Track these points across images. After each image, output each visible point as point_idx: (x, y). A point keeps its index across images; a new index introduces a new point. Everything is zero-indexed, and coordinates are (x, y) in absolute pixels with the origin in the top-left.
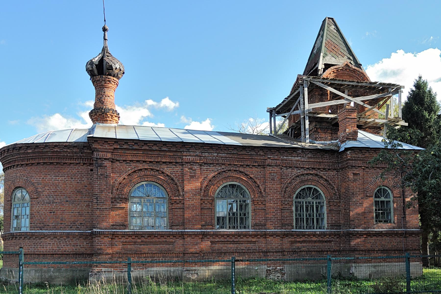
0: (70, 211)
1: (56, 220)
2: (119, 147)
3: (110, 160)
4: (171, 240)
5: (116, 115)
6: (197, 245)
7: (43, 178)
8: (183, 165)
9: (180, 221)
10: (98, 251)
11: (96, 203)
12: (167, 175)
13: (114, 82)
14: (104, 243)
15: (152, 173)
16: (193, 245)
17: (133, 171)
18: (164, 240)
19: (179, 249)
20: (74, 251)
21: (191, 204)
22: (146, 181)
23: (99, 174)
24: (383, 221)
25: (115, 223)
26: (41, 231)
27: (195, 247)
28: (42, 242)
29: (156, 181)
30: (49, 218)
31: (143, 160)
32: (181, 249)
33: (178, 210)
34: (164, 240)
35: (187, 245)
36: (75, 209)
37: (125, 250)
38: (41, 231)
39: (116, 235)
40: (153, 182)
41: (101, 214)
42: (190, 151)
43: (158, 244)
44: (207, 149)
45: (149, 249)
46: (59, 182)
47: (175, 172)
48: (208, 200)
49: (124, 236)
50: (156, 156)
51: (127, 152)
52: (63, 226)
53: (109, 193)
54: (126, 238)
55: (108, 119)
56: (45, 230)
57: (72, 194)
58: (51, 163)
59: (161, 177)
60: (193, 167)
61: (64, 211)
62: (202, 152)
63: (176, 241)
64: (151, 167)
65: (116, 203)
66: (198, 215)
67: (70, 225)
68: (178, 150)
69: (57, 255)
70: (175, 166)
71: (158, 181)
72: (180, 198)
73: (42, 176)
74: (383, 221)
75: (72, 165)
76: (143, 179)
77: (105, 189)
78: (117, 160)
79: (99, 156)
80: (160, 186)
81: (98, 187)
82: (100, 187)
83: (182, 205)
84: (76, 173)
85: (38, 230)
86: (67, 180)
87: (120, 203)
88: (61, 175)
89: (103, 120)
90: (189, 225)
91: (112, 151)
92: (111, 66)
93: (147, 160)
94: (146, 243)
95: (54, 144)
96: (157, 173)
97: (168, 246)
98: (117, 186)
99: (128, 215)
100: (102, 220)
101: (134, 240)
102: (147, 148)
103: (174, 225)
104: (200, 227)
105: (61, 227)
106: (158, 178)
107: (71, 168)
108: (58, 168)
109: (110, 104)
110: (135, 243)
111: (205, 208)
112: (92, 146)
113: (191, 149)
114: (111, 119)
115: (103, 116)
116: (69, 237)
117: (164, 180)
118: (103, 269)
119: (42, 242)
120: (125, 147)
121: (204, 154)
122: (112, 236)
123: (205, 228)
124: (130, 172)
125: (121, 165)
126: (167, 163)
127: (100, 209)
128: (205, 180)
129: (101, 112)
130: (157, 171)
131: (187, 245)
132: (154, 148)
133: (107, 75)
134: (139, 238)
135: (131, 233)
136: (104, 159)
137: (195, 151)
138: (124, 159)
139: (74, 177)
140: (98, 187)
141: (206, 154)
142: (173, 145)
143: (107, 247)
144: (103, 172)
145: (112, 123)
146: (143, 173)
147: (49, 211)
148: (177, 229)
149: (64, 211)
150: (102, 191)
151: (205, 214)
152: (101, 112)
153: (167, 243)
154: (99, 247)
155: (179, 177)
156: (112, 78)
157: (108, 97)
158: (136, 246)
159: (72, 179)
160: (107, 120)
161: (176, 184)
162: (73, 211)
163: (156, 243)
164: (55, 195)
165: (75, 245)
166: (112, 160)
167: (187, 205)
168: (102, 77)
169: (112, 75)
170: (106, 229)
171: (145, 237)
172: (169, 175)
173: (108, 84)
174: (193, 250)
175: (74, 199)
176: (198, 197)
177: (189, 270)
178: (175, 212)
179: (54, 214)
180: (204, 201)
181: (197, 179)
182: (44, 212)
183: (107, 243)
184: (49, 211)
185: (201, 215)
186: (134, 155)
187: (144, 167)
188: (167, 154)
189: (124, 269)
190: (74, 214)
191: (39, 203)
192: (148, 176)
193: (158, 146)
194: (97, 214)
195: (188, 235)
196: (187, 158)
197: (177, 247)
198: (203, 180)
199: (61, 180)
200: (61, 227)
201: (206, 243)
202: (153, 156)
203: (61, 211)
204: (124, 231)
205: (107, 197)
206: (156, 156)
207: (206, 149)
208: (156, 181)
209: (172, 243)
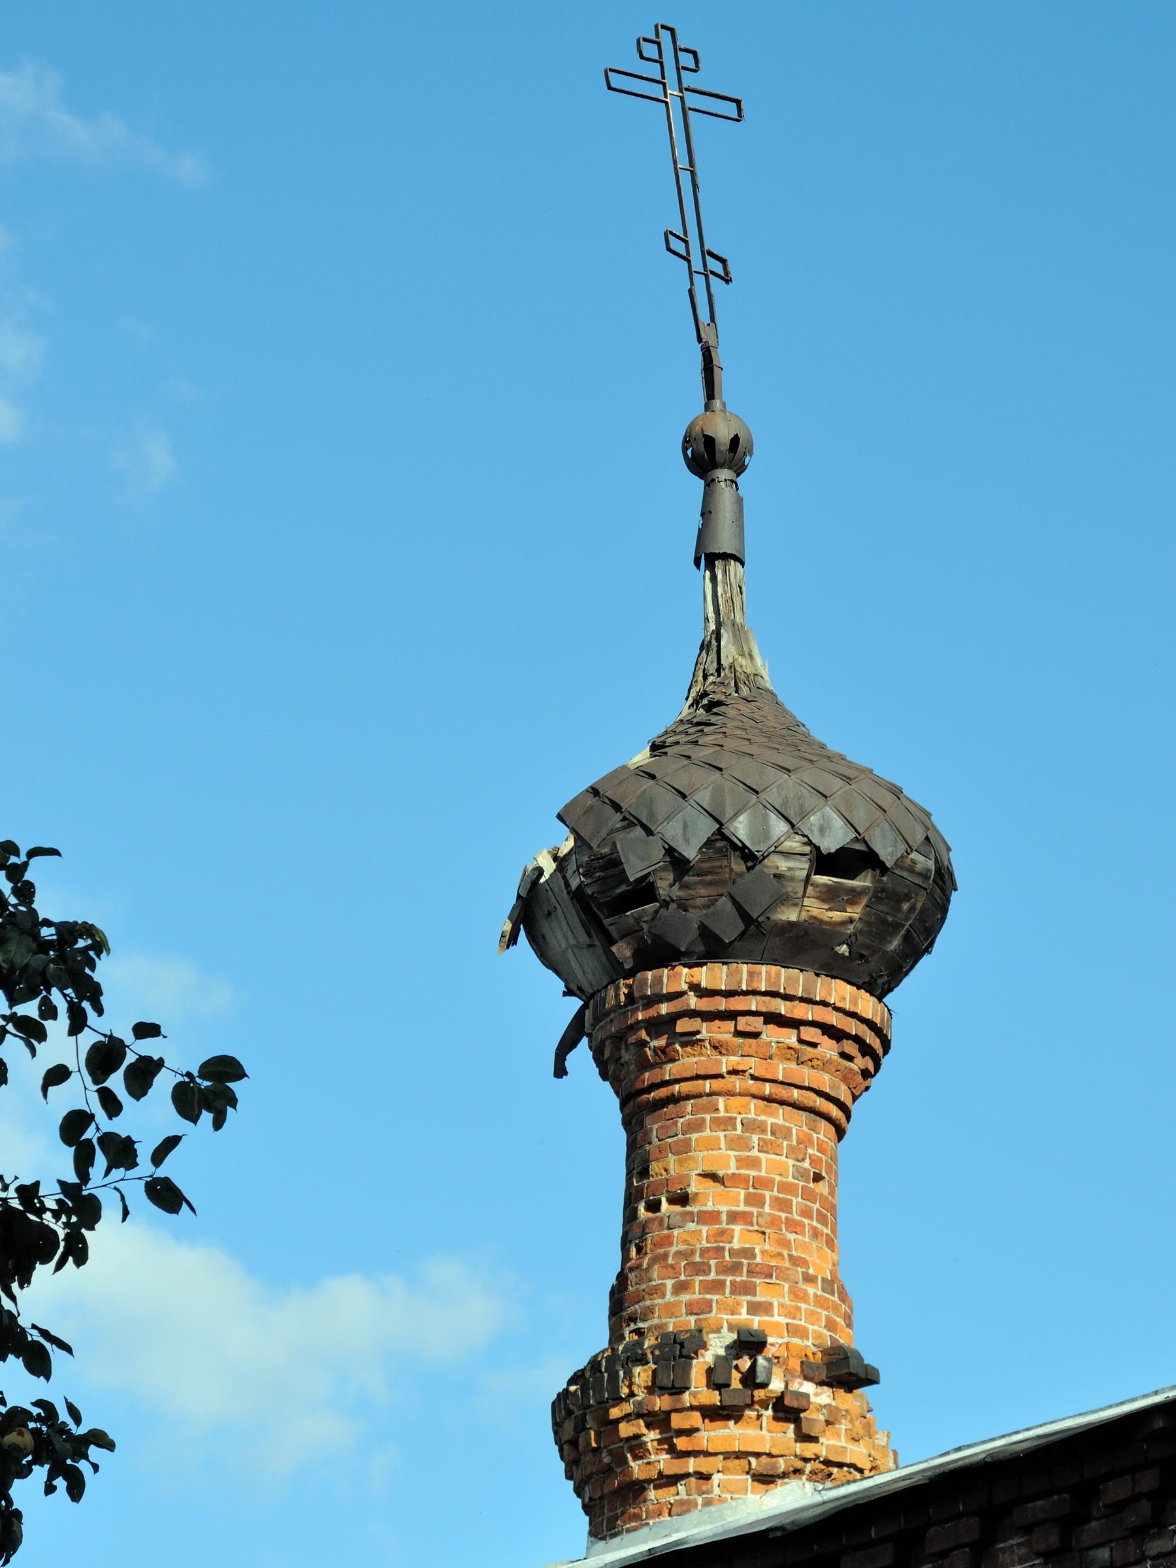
5: (714, 1398)
24: (724, 1217)
55: (637, 1469)
74: (724, 1217)
109: (680, 1288)
114: (663, 1461)
145: (685, 1507)
156: (679, 977)
157: (682, 1199)
160: (637, 1489)
173: (665, 1055)
185: (601, 1498)
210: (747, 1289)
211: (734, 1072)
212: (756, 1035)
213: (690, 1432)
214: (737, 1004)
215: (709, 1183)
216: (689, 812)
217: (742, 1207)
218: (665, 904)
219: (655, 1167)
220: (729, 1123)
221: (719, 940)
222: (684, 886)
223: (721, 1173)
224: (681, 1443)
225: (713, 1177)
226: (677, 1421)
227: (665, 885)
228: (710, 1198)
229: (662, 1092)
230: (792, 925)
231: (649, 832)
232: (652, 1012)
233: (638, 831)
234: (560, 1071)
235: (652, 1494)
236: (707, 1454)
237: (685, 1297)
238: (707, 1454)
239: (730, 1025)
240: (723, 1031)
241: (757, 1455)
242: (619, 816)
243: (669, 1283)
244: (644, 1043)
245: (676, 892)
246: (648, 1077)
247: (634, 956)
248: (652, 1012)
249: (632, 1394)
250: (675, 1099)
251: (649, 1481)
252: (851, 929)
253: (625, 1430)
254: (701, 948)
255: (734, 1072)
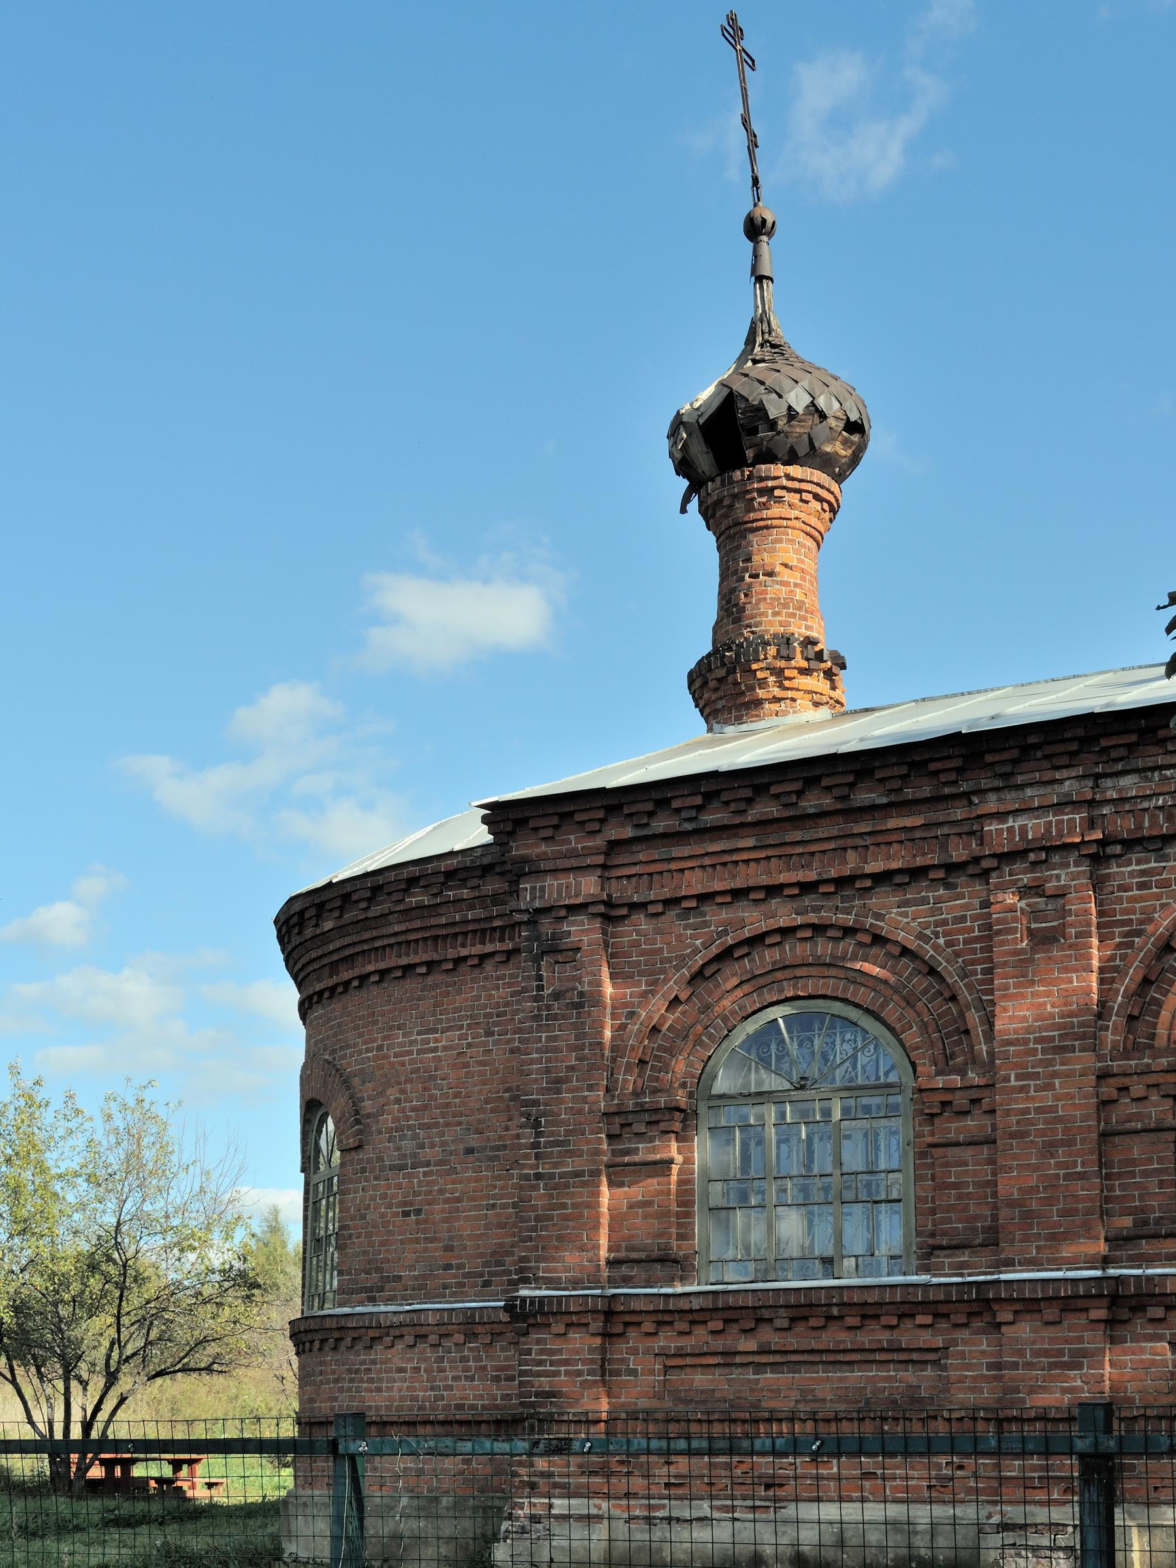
0: (481, 1199)
1: (426, 1250)
2: (629, 832)
3: (593, 909)
4: (925, 1338)
5: (804, 664)
6: (1079, 1366)
7: (380, 1048)
8: (985, 874)
9: (976, 1218)
10: (541, 1405)
11: (535, 1145)
12: (905, 951)
13: (799, 491)
14: (566, 1362)
15: (824, 948)
16: (1053, 1366)
17: (714, 950)
18: (884, 1337)
19: (972, 1390)
20: (496, 1407)
21: (1038, 1110)
22: (787, 1000)
23: (547, 992)
25: (628, 1249)
26: (370, 1309)
27: (1067, 1379)
28: (374, 1362)
29: (845, 989)
30: (402, 1242)
31: (764, 880)
32: (987, 1394)
33: (967, 1153)
34: (884, 1337)
35: (1015, 1366)
36: (501, 1188)
37: (679, 1400)
38: (370, 1309)
39: (627, 1318)
40: (828, 1003)
41: (554, 1207)
42: (1020, 779)
43: (681, 1367)
44: (1122, 752)
45: (803, 1392)
46: (439, 1059)
47: (945, 922)
48: (1147, 1071)
49: (667, 1318)
50: (833, 845)
51: (676, 852)
52: (455, 1277)
53: (591, 1088)
54: (681, 1333)
55: (761, 693)
56: (389, 1300)
57: (493, 1110)
58: (408, 969)
59: (868, 967)
60: (1048, 879)
61: (459, 1200)
62: (1097, 777)
63: (955, 1343)
64: (812, 918)
65: (630, 1141)
66: (1081, 1176)
67: (481, 1275)
68: (947, 791)
69: (428, 1427)
70: (948, 886)
71: (855, 994)
72: (974, 1077)
73: (374, 1041)
75: (489, 966)
76: (770, 992)
77: (572, 1068)
78: (634, 907)
79: (542, 897)
80: (867, 1022)
81: (540, 1061)
82: (549, 1060)
83: (987, 1121)
84: (507, 1004)
85: (361, 1303)
86: (469, 1045)
87: (652, 1140)
88: (448, 1020)
89: (739, 707)
90: (1026, 1239)
91: (600, 859)
92: (761, 410)
93: (783, 878)
94: (784, 1360)
95: (405, 873)
96: (849, 945)
97: (909, 1376)
98: (633, 1048)
99: (692, 1203)
100: (560, 1238)
101: (719, 1344)
102: (772, 810)
103: (941, 1248)
104: (1102, 1247)
105: (445, 1287)
106: (850, 974)
107: (486, 978)
108: (436, 986)
109: (775, 614)
110: (729, 1360)
111: (1128, 1126)
112: (510, 851)
113: (1024, 766)
114: (776, 692)
115: (736, 684)
116: (475, 1335)
117: (885, 982)
118: (560, 1505)
119: (374, 1362)
120: (661, 824)
121: (1109, 782)
122: (606, 1322)
123: (1131, 1258)
124: (699, 960)
125: (658, 931)
126: (898, 879)
127: (551, 1176)
128: (1130, 945)
129: (723, 665)
130: (849, 931)
131: (1015, 1366)
132: (812, 802)
133: (753, 465)
134: (745, 1331)
135: (696, 1304)
136: (566, 906)
137: (1048, 776)
138: (667, 893)
139: (497, 1024)
140: (540, 1061)
141: (1126, 781)
142: (909, 764)
143: (583, 1383)
144: (568, 979)
145: (785, 713)
146: (769, 956)
147: (399, 1205)
148: (959, 1268)
149: (459, 1200)
150: (557, 1084)
151: (1133, 1162)
152: (723, 665)
153: (903, 1356)
154: (544, 1383)
155: (974, 951)
156: (778, 469)
157: (770, 574)
158: (736, 1374)
159: (489, 1033)
160: (758, 703)
161: (953, 998)
162: (495, 1197)
163: (841, 1357)
164: (422, 1126)
165: (502, 1374)
166: (601, 909)
167: (1014, 1119)
168: (731, 482)
169: (782, 453)
170: (576, 1283)
171: (778, 1323)
172: (913, 944)
173: (765, 506)
174: (1053, 1398)
175: (500, 1138)
176: (1083, 1060)
177: (1024, 1527)
178: (947, 1164)
179: (418, 1223)
180: (1126, 1081)
181: (1071, 947)
182: (383, 1215)
183: (584, 1363)
184: (399, 1205)
186: (720, 863)
187: (773, 924)
188: (892, 823)
189: (663, 1507)
190: (499, 1215)
191: (364, 1170)
192: (799, 972)
193: (828, 789)
194: (534, 1208)
195: (1018, 1307)
196: (1010, 830)
197: (962, 1379)
198: (1119, 946)
199: (445, 1048)
200: (445, 1287)
201: (1142, 1351)
202: (813, 848)
203: (447, 1201)
204: (669, 1291)
205: (580, 1111)
206: (833, 845)
207: (1114, 754)
208: (845, 989)
209: (934, 1357)
210: (804, 618)
211: (797, 518)
212: (807, 502)
213: (790, 679)
214: (804, 486)
215: (783, 567)
216: (798, 389)
217: (799, 582)
218: (779, 433)
219: (755, 558)
220: (792, 541)
221: (797, 455)
222: (791, 426)
223: (790, 564)
224: (787, 683)
225: (786, 565)
226: (787, 673)
227: (781, 423)
228: (785, 575)
229: (761, 523)
230: (828, 453)
231: (780, 396)
232: (763, 485)
233: (774, 396)
234: (683, 510)
235: (767, 706)
236: (798, 690)
237: (778, 618)
238: (798, 690)
239: (798, 496)
240: (794, 498)
241: (816, 693)
242: (763, 387)
243: (770, 611)
244: (755, 499)
245: (786, 428)
246: (752, 516)
247: (754, 457)
248: (763, 485)
249: (766, 658)
250: (767, 527)
251: (766, 700)
252: (843, 461)
253: (760, 675)
254: (786, 458)
255: (797, 518)
